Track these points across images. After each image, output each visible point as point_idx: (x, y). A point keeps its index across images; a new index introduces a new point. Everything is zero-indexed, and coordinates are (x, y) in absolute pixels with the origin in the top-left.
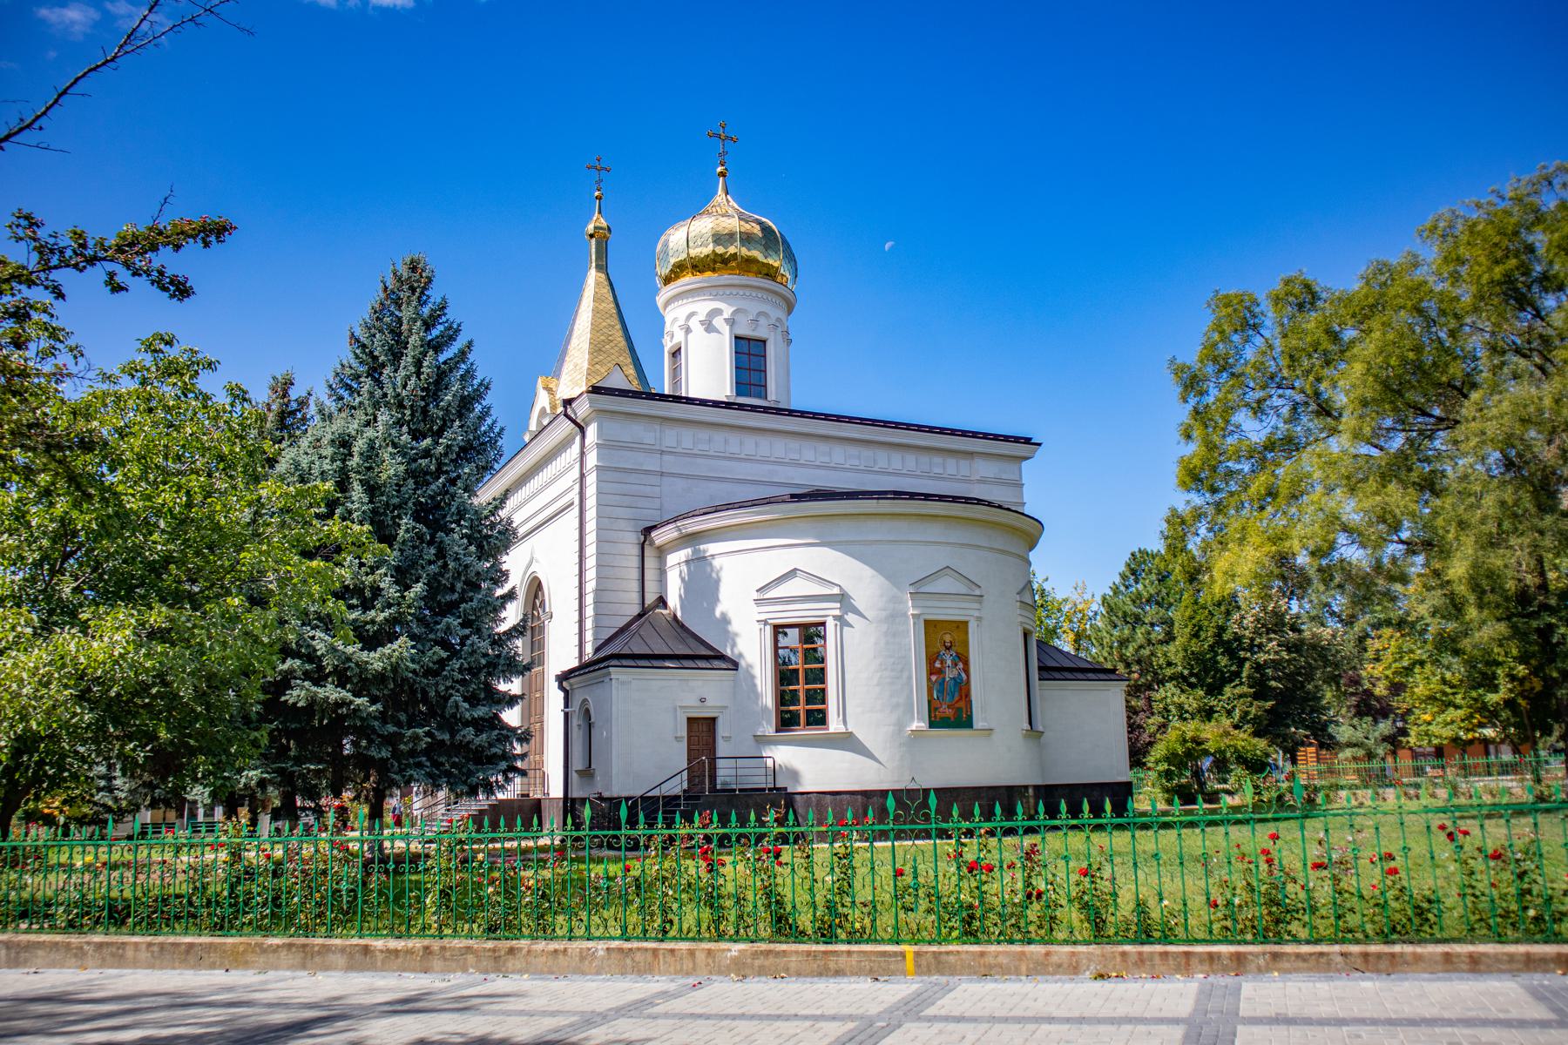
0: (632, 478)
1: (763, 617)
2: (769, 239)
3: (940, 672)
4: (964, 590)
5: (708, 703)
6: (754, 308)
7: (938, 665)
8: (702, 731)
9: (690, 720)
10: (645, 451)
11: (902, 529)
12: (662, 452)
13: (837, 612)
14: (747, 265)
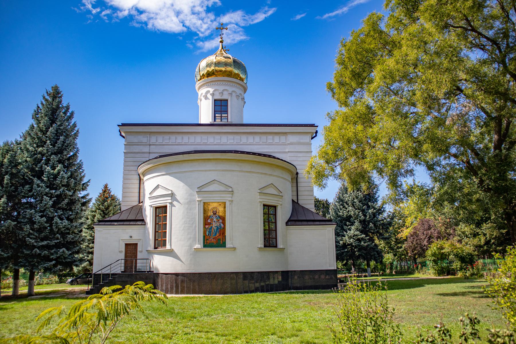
0: (138, 155)
1: (261, 200)
2: (236, 64)
3: (210, 224)
4: (222, 188)
5: (133, 238)
6: (221, 88)
7: (209, 221)
8: (131, 249)
9: (126, 244)
10: (143, 145)
11: (247, 167)
12: (150, 145)
13: (170, 201)
14: (230, 74)
